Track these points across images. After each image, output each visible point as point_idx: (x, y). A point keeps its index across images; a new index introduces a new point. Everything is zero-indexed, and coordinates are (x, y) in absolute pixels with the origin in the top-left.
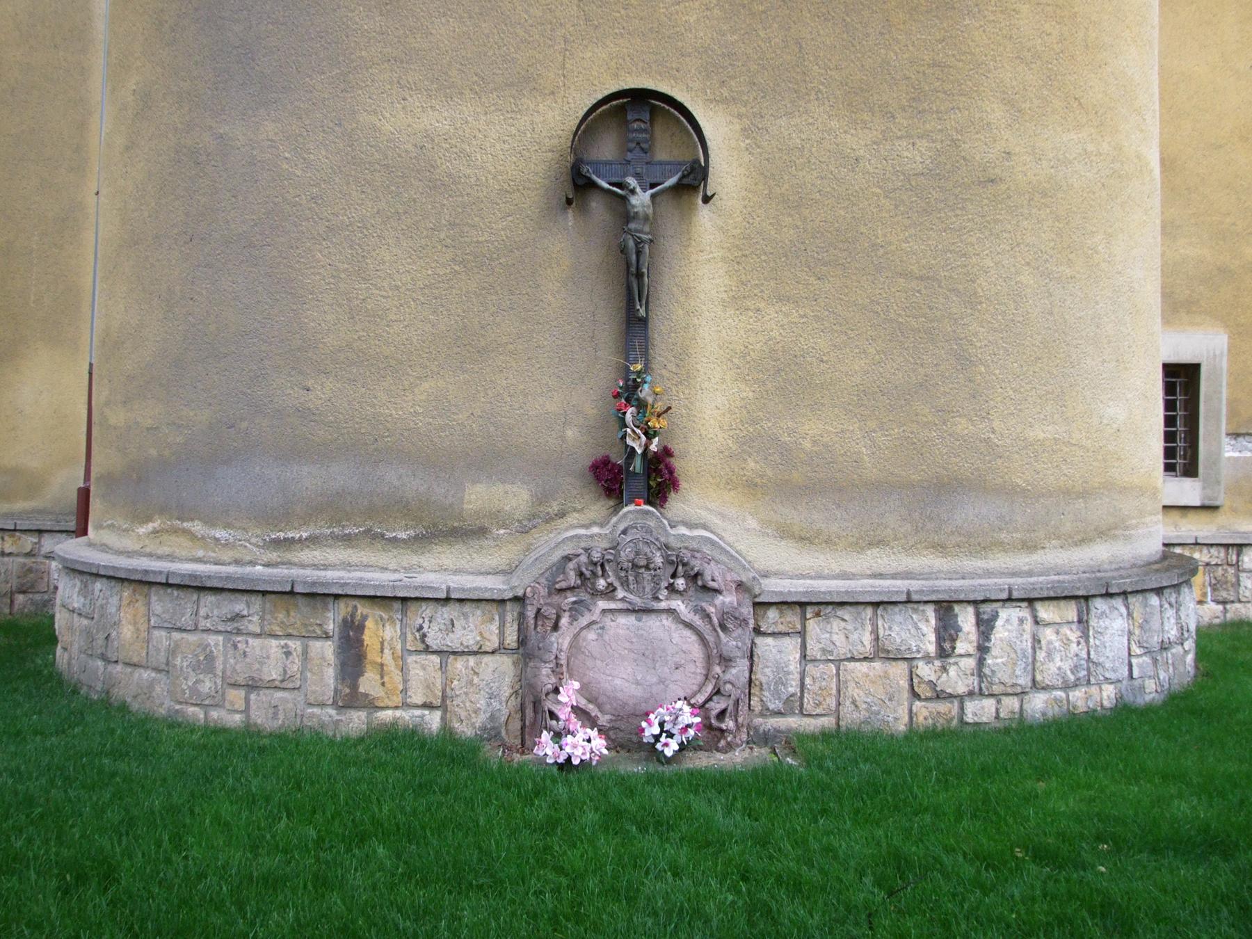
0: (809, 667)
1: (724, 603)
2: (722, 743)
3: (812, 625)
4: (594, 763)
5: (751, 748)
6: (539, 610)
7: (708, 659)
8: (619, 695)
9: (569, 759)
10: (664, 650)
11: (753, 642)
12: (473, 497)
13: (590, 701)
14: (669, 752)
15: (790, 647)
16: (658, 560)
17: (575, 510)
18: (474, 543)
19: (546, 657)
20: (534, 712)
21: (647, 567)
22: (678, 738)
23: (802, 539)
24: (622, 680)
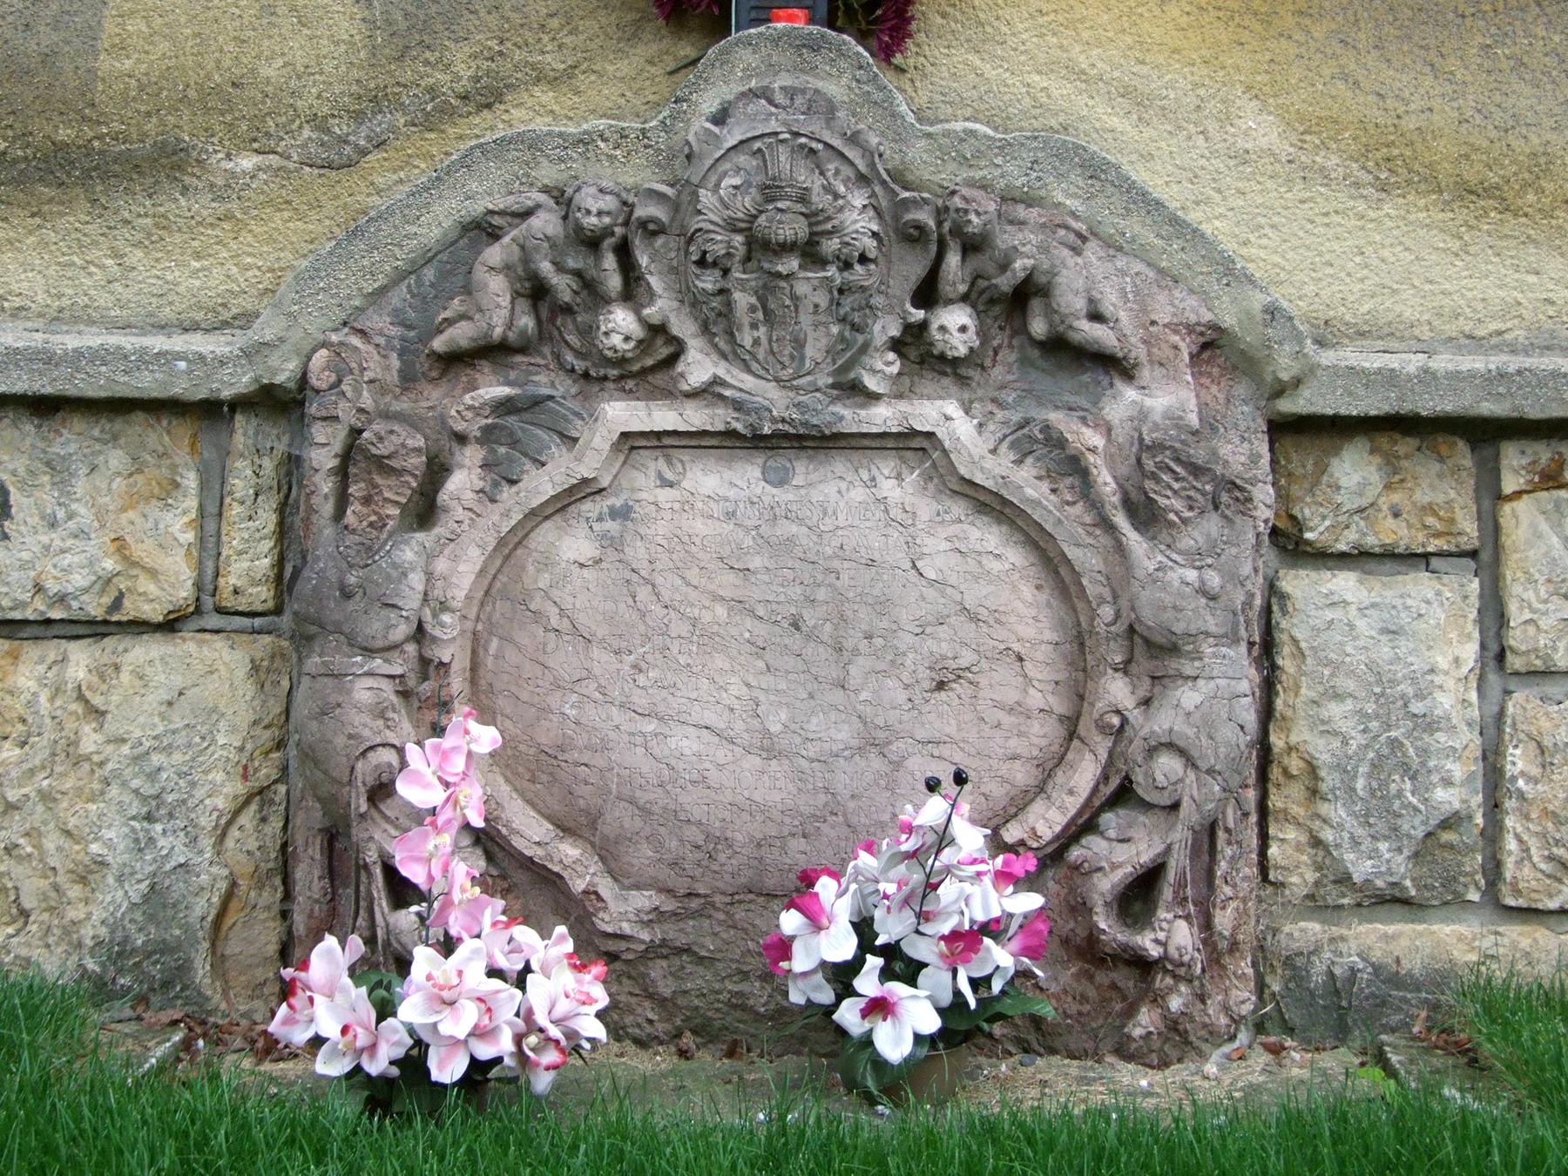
0: (1521, 702)
1: (1142, 415)
2: (1145, 1021)
3: (1529, 525)
4: (542, 1082)
5: (1276, 1050)
6: (356, 432)
8: (692, 802)
9: (414, 1063)
10: (882, 605)
11: (1272, 589)
12: (136, 25)
13: (566, 829)
14: (893, 1043)
15: (1439, 610)
16: (858, 221)
17: (541, 77)
18: (135, 207)
19: (374, 626)
20: (328, 862)
21: (810, 253)
22: (936, 980)
23: (1468, 192)
24: (699, 731)
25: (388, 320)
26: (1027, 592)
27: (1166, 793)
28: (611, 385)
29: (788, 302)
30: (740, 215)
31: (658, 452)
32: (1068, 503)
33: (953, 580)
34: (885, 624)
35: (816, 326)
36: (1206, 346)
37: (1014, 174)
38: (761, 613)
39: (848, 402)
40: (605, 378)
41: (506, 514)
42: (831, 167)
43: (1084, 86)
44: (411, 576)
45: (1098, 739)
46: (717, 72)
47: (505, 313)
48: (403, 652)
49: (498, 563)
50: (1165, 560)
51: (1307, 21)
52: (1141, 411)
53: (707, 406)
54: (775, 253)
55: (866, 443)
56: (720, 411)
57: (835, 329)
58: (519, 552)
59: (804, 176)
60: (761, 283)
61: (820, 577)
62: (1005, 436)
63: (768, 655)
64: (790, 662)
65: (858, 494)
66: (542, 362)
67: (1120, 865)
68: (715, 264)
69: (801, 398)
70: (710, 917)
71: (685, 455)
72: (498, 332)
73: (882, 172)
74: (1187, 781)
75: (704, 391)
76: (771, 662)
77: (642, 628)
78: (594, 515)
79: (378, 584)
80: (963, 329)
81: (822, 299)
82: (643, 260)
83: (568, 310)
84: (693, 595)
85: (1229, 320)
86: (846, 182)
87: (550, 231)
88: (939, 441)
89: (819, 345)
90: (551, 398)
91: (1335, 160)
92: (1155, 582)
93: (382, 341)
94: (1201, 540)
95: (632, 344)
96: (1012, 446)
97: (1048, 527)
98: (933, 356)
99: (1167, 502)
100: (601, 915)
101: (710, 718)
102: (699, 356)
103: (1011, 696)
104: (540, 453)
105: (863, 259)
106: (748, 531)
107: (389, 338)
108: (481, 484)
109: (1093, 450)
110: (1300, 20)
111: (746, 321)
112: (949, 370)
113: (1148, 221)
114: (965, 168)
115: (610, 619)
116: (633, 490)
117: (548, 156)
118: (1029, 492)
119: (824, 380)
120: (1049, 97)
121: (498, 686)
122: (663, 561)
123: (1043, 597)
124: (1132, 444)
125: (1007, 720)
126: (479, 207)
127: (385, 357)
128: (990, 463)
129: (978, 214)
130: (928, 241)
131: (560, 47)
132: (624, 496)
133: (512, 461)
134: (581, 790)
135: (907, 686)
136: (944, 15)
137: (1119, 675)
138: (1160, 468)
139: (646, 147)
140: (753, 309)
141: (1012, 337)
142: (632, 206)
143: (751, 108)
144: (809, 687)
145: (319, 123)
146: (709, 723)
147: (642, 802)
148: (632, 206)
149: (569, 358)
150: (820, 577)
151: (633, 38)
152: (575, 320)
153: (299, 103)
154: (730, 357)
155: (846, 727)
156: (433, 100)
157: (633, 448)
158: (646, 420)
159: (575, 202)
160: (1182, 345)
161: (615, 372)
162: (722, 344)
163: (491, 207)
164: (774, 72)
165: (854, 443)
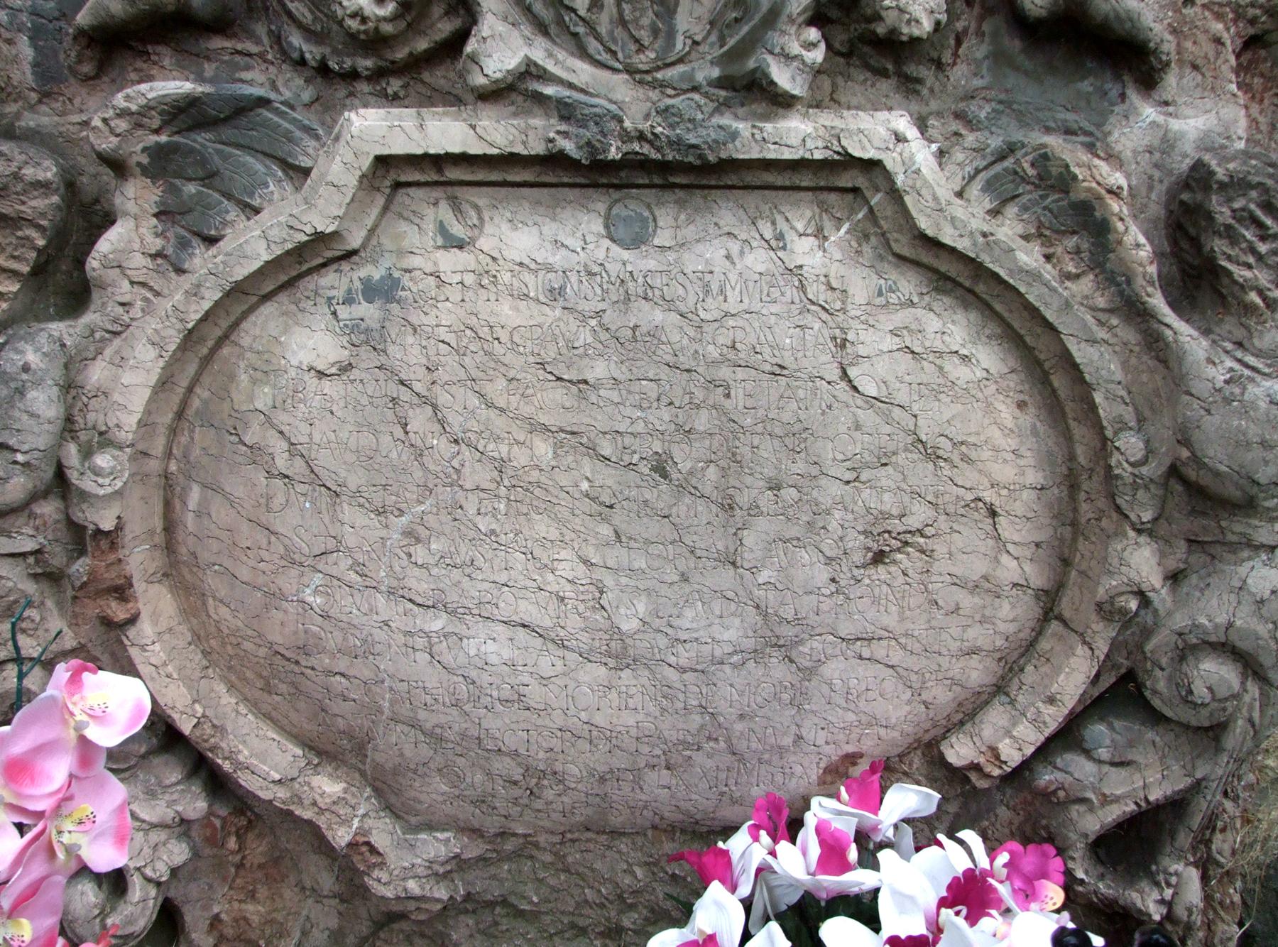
1: (1167, 143)
7: (1082, 494)
8: (503, 726)
10: (797, 439)
26: (1006, 412)
27: (1204, 712)
28: (364, 87)
31: (438, 193)
33: (902, 396)
34: (800, 467)
38: (607, 452)
40: (352, 75)
41: (195, 293)
45: (1098, 626)
48: (32, 516)
49: (192, 369)
50: (1237, 366)
52: (1164, 139)
53: (515, 115)
55: (770, 178)
56: (537, 122)
58: (225, 351)
61: (699, 395)
63: (618, 518)
64: (653, 528)
65: (758, 260)
66: (254, 49)
67: (1117, 799)
69: (670, 102)
70: (532, 857)
71: (481, 197)
74: (1247, 698)
76: (623, 527)
77: (418, 474)
78: (339, 294)
84: (499, 423)
90: (264, 102)
92: (1228, 401)
96: (989, 187)
97: (1050, 315)
100: (376, 873)
101: (528, 610)
102: (501, 27)
103: (976, 567)
104: (251, 195)
106: (584, 319)
108: (157, 244)
109: (1115, 192)
115: (368, 459)
116: (401, 253)
119: (706, 72)
121: (205, 556)
122: (450, 368)
123: (1027, 419)
124: (1151, 188)
125: (968, 601)
128: (958, 209)
132: (387, 262)
133: (208, 207)
134: (337, 707)
135: (829, 560)
137: (1143, 539)
138: (1239, 221)
141: (981, 19)
144: (682, 565)
146: (527, 619)
147: (428, 726)
149: (296, 40)
150: (699, 395)
154: (553, 30)
155: (737, 621)
157: (398, 185)
158: (416, 134)
160: (1226, 38)
161: (369, 63)
165: (750, 178)
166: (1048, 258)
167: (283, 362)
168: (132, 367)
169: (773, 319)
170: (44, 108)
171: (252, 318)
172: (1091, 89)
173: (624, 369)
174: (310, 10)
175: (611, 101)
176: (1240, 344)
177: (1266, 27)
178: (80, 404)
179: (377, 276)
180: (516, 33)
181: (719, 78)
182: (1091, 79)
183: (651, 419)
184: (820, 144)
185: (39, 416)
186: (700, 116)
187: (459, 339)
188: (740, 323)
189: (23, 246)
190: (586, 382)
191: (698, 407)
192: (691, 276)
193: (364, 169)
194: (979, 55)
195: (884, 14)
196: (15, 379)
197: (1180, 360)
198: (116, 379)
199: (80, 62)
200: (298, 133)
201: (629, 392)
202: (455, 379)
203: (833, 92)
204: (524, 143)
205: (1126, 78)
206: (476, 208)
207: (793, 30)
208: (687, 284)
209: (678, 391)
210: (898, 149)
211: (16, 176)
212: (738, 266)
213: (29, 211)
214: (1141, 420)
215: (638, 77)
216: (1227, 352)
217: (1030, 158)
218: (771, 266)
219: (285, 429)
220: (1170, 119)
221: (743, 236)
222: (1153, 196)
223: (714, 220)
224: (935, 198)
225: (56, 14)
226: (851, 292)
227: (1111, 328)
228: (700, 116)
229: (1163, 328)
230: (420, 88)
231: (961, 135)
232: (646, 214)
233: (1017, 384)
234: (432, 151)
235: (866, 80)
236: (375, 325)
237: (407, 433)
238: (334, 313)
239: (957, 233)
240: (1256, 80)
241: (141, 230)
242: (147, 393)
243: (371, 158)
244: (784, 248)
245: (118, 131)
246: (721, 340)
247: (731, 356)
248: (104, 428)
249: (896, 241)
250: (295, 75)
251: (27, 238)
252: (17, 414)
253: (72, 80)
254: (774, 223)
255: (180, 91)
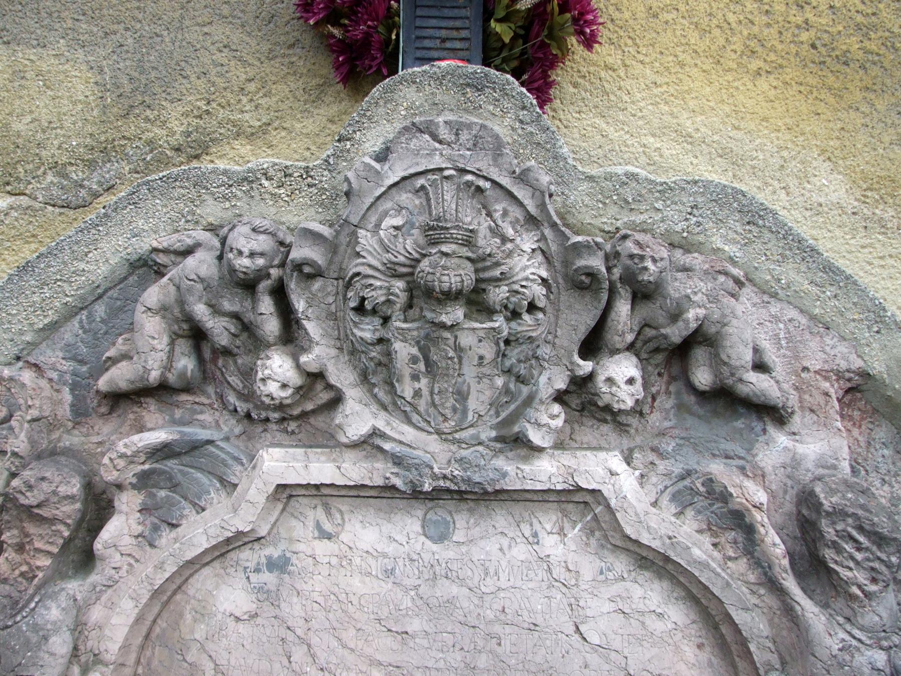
1: (795, 462)
16: (527, 268)
21: (476, 301)
25: (61, 354)
26: (689, 651)
29: (451, 354)
30: (401, 259)
31: (316, 501)
32: (730, 559)
33: (617, 644)
35: (480, 378)
36: (848, 391)
37: (675, 219)
39: (510, 454)
41: (160, 567)
42: (499, 207)
43: (689, 147)
44: (53, 639)
46: (381, 110)
47: (163, 356)
49: (156, 610)
50: (847, 638)
51: (872, 96)
52: (793, 459)
53: (366, 457)
54: (439, 301)
55: (529, 496)
56: (379, 465)
57: (499, 382)
58: (178, 597)
59: (471, 217)
60: (422, 333)
62: (666, 488)
65: (521, 552)
66: (206, 401)
68: (374, 311)
69: (464, 453)
71: (344, 505)
72: (154, 376)
73: (553, 213)
75: (364, 442)
78: (251, 565)
79: (14, 652)
80: (631, 381)
81: (488, 351)
82: (299, 305)
83: (227, 352)
84: (350, 658)
85: (877, 367)
86: (513, 224)
87: (204, 271)
88: (605, 499)
89: (482, 398)
90: (210, 442)
91: (891, 212)
93: (54, 375)
94: (884, 615)
95: (290, 391)
96: (674, 498)
98: (596, 405)
99: (849, 574)
102: (358, 407)
104: (199, 498)
105: (532, 307)
106: (407, 590)
107: (62, 373)
108: (139, 529)
109: (758, 507)
110: (865, 95)
111: (407, 372)
112: (609, 418)
113: (803, 268)
114: (625, 212)
116: (291, 540)
117: (213, 194)
118: (697, 552)
119: (487, 434)
120: (661, 156)
123: (705, 656)
124: (785, 492)
126: (145, 244)
127: (58, 391)
129: (654, 261)
130: (599, 290)
131: (256, 107)
132: (282, 546)
133: (173, 505)
136: (575, 85)
138: (842, 537)
139: (309, 186)
140: (414, 360)
141: (669, 383)
142: (289, 246)
143: (414, 144)
145: (59, 169)
148: (289, 246)
149: (232, 399)
150: (481, 643)
151: (317, 100)
152: (235, 362)
153: (44, 153)
154: (390, 408)
156: (151, 151)
158: (302, 472)
159: (228, 242)
160: (832, 391)
162: (381, 395)
163: (155, 244)
164: (434, 109)
165: (515, 496)
166: (715, 545)
167: (214, 609)
168: (117, 613)
169: (530, 593)
170: (76, 432)
171: (196, 576)
172: (743, 426)
173: (431, 625)
174: (242, 381)
175: (426, 452)
176: (848, 619)
177: (858, 382)
178: (83, 637)
179: (276, 556)
180: (367, 410)
181: (496, 437)
182: (743, 420)
183: (449, 659)
184: (561, 479)
185: (55, 655)
186: (483, 463)
187: (326, 601)
188: (508, 595)
189: (55, 535)
190: (407, 633)
191: (480, 652)
192: (476, 562)
193: (270, 493)
194: (668, 406)
195: (602, 395)
196: (43, 629)
197: (807, 631)
198: (108, 618)
199: (99, 406)
200: (230, 462)
201: (434, 641)
202: (323, 628)
203: (572, 433)
204: (370, 478)
205: (766, 419)
206: (341, 512)
207: (543, 408)
208: (474, 568)
209: (467, 641)
210: (612, 481)
211: (55, 493)
212: (508, 556)
213: (61, 514)
214: (783, 663)
215: (444, 436)
216: (840, 625)
217: (701, 480)
218: (529, 557)
219: (213, 654)
220: (797, 444)
221: (511, 535)
222: (788, 497)
223: (493, 523)
224: (637, 514)
225: (87, 375)
226: (581, 573)
227: (760, 596)
228: (483, 463)
229: (795, 603)
230: (308, 427)
231: (655, 464)
232: (449, 518)
233: (696, 631)
234: (312, 483)
235: (592, 426)
236: (273, 588)
237: (290, 662)
238: (248, 578)
239: (651, 537)
240: (855, 413)
241: (129, 521)
242: (127, 629)
243: (274, 486)
244: (538, 543)
245: (119, 467)
246: (495, 606)
247: (502, 617)
248: (97, 652)
249: (612, 536)
250: (231, 417)
251: (58, 531)
252: (41, 654)
253: (94, 415)
254: (531, 525)
255: (158, 440)
